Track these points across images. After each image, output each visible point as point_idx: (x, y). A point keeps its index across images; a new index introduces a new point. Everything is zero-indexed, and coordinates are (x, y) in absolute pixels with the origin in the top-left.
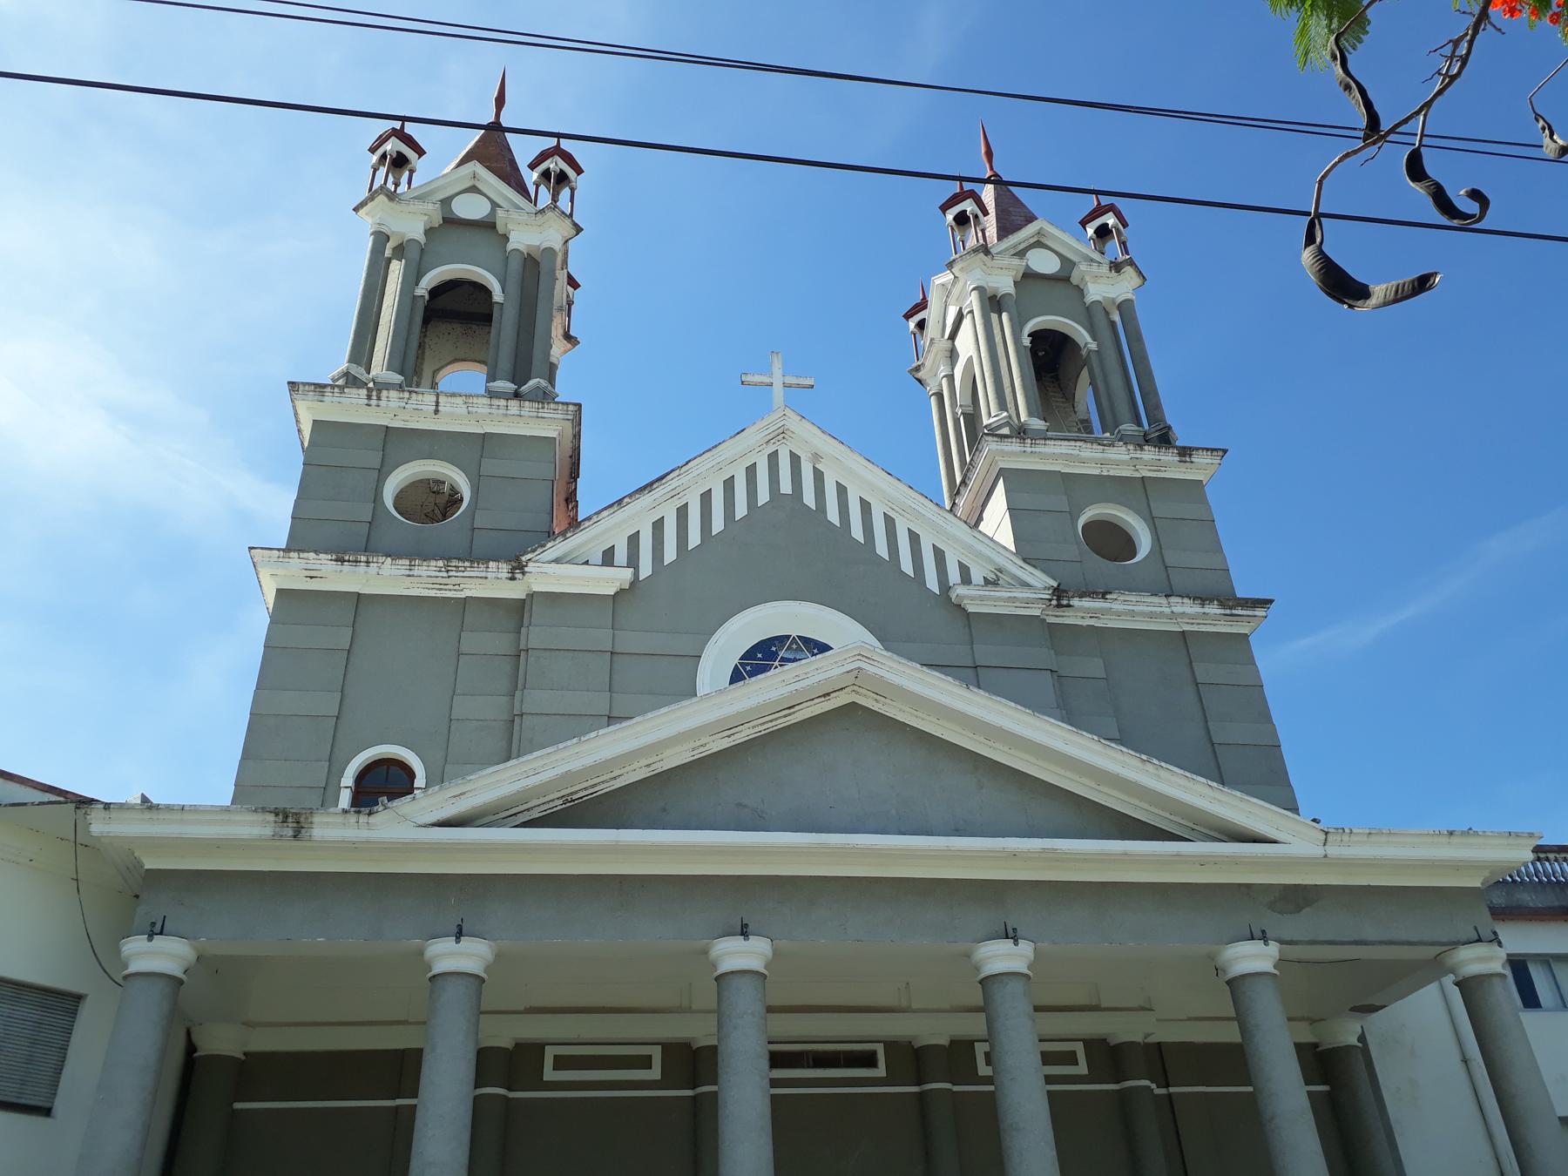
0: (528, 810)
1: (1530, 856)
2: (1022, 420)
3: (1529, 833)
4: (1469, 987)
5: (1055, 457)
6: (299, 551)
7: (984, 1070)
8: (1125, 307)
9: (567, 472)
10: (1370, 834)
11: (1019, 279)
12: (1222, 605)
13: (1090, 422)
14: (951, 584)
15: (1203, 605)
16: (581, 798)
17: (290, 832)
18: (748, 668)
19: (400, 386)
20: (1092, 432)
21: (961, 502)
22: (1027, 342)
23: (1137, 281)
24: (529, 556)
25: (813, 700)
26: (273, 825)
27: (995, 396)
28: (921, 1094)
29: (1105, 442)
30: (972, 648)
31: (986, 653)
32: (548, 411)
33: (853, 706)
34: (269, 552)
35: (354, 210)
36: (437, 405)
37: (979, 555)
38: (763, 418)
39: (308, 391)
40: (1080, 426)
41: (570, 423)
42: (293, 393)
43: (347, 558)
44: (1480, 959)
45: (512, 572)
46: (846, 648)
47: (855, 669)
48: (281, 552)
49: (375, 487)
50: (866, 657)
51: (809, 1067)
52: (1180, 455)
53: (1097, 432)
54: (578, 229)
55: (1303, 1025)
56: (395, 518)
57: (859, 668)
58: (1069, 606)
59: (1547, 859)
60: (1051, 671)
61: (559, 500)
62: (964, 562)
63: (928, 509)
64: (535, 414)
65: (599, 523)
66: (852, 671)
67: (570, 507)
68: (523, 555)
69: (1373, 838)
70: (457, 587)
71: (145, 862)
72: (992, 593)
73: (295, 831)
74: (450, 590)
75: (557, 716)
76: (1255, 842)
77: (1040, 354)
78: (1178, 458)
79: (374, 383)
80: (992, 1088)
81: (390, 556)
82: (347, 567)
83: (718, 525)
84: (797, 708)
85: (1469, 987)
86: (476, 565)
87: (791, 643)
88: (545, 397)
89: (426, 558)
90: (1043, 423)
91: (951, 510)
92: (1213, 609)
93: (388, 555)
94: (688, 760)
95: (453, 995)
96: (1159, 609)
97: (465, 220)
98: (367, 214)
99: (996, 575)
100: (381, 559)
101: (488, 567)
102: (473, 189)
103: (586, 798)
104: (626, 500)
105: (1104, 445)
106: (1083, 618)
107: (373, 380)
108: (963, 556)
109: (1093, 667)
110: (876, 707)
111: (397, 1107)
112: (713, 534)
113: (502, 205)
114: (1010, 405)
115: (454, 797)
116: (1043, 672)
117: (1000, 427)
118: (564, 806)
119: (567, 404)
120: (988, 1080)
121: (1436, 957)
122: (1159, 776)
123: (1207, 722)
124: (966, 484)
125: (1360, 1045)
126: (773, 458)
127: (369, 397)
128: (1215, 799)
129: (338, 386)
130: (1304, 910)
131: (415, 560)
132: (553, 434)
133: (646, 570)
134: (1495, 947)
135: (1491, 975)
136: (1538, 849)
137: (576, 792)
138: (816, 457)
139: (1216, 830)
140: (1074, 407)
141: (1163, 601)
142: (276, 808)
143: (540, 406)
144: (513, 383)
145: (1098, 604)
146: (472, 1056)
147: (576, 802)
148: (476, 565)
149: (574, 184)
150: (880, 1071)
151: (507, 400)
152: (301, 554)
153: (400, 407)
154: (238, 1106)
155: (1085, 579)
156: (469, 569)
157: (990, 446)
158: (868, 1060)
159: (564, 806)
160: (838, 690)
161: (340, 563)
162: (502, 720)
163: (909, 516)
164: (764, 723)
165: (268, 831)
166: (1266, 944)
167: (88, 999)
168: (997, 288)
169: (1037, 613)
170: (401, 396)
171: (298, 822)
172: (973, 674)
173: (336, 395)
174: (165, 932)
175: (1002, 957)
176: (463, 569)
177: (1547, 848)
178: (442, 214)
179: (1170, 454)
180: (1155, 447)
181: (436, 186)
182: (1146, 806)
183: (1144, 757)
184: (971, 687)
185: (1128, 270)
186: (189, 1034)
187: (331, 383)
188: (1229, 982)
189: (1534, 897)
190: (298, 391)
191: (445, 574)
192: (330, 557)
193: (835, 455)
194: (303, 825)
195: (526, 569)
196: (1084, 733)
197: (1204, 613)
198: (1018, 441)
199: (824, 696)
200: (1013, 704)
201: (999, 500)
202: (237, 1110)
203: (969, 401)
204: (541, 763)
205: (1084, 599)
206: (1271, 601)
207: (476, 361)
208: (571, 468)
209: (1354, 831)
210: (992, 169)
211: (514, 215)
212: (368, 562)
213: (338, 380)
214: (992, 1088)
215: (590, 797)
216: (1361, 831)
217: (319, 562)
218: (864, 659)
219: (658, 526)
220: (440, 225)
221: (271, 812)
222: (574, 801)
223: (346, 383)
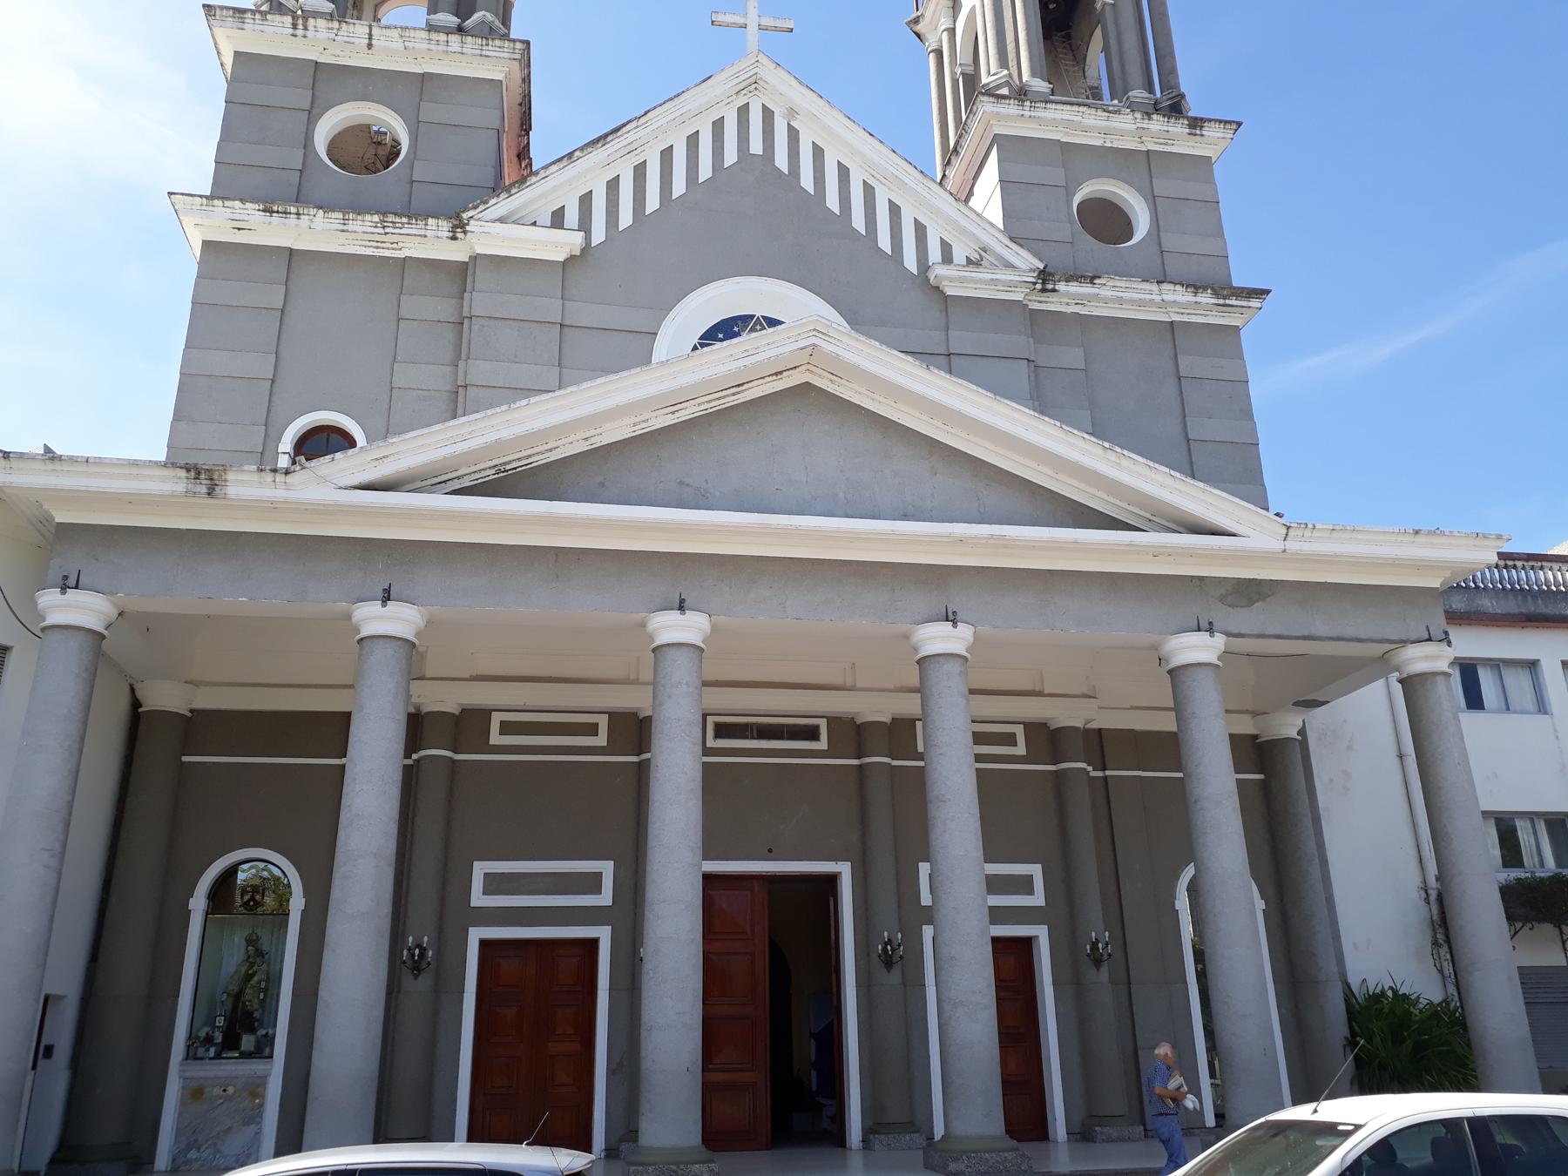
0: (458, 478)
1: (1494, 559)
2: (1024, 80)
3: (1496, 535)
4: (1413, 686)
5: (1055, 123)
6: (223, 198)
9: (517, 122)
10: (1333, 530)
12: (1216, 294)
13: (1101, 90)
14: (930, 264)
15: (1196, 293)
16: (515, 468)
17: (204, 490)
19: (331, 15)
20: (1101, 99)
21: (951, 173)
24: (470, 213)
25: (763, 378)
28: (860, 766)
29: (1111, 108)
31: (960, 340)
32: (495, 48)
33: (807, 386)
34: (191, 198)
36: (370, 39)
37: (964, 231)
39: (227, 17)
40: (1089, 92)
41: (517, 64)
42: (209, 18)
43: (275, 208)
44: (1427, 658)
45: (454, 229)
46: (800, 322)
47: (810, 346)
48: (204, 199)
49: (305, 130)
51: (753, 738)
52: (1190, 126)
53: (1106, 100)
55: (1247, 718)
57: (814, 345)
59: (1515, 567)
60: (1028, 360)
61: (508, 156)
62: (948, 240)
63: (911, 177)
64: (478, 52)
65: (546, 179)
66: (805, 347)
67: (523, 166)
68: (463, 212)
69: (1335, 534)
70: (395, 246)
71: (53, 513)
72: (973, 275)
73: (209, 489)
74: (388, 249)
75: (504, 390)
76: (1213, 534)
77: (1051, 7)
78: (1188, 131)
79: (302, 11)
80: (921, 764)
82: (276, 218)
83: (679, 187)
85: (1413, 686)
86: (414, 221)
87: (755, 324)
88: (498, 31)
89: (360, 211)
90: (1046, 84)
91: (941, 183)
92: (1206, 298)
95: (381, 657)
99: (980, 255)
100: (313, 211)
101: (426, 225)
103: (520, 469)
104: (577, 154)
105: (1109, 112)
106: (1068, 304)
107: (301, 8)
109: (1072, 357)
110: (831, 388)
112: (673, 198)
114: (1012, 63)
115: (377, 459)
116: (1020, 361)
117: (999, 87)
118: (496, 476)
121: (1383, 656)
123: (1185, 417)
125: (1299, 738)
126: (743, 111)
127: (295, 26)
128: (1176, 489)
129: (260, 12)
130: (1255, 605)
131: (349, 213)
132: (499, 76)
133: (598, 235)
134: (1444, 645)
135: (1434, 674)
136: (1501, 555)
137: (510, 462)
138: (792, 112)
140: (1084, 72)
141: (1154, 287)
142: (187, 464)
143: (484, 43)
144: (456, 16)
145: (1086, 289)
146: (403, 718)
147: (510, 472)
148: (414, 221)
151: (447, 34)
152: (226, 202)
154: (185, 759)
155: (1074, 262)
156: (406, 226)
157: (986, 106)
158: (811, 733)
159: (496, 476)
160: (791, 369)
161: (268, 214)
163: (890, 185)
164: (711, 401)
165: (180, 487)
167: (14, 650)
169: (1019, 297)
170: (330, 25)
171: (211, 479)
172: (947, 360)
173: (257, 22)
174: (80, 586)
175: (938, 638)
176: (400, 225)
177: (1516, 556)
179: (1180, 125)
180: (1164, 116)
182: (1105, 496)
183: (1107, 445)
184: (931, 368)
186: (133, 690)
187: (254, 8)
188: (1170, 672)
189: (1495, 604)
190: (214, 15)
191: (381, 231)
192: (256, 207)
193: (813, 110)
194: (217, 482)
195: (468, 228)
196: (1046, 419)
197: (1196, 302)
198: (1016, 102)
199: (776, 374)
200: (974, 387)
202: (185, 762)
203: (970, 60)
204: (468, 429)
205: (1071, 284)
206: (1267, 292)
208: (522, 118)
209: (1317, 527)
212: (298, 214)
214: (921, 764)
215: (524, 468)
216: (1324, 527)
218: (820, 335)
219: (613, 185)
221: (181, 468)
222: (507, 471)
223: (270, 9)
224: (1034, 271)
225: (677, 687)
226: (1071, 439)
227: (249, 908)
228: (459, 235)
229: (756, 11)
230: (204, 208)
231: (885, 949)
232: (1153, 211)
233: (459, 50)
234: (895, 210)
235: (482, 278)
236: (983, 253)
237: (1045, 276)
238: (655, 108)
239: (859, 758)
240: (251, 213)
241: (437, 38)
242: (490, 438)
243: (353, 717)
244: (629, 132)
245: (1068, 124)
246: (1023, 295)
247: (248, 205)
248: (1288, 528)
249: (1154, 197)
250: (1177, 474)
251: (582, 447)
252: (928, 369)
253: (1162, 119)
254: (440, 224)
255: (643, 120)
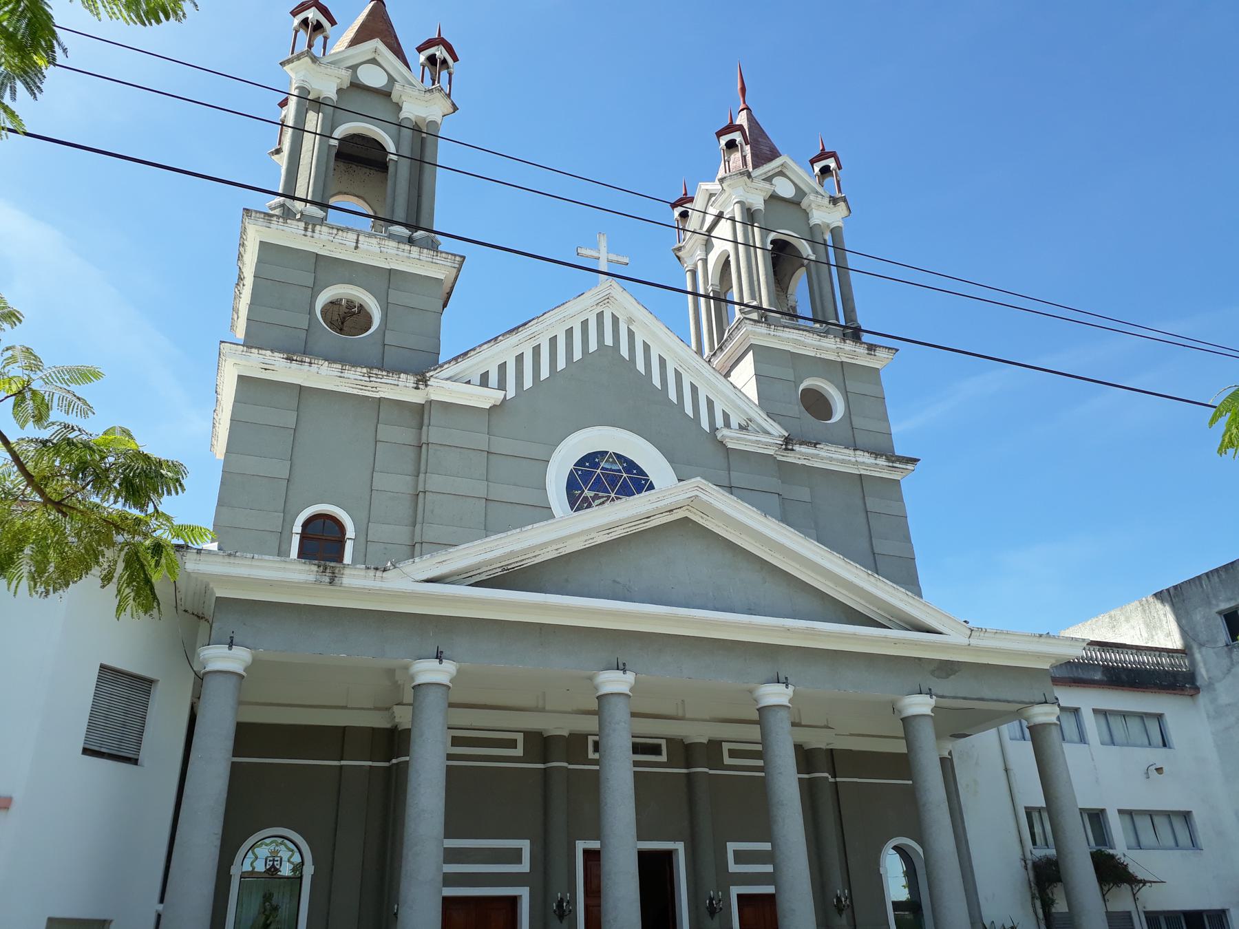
0: (479, 574)
7: (592, 755)
8: (835, 232)
11: (767, 198)
12: (888, 460)
15: (876, 458)
16: (513, 568)
17: (327, 580)
18: (580, 473)
22: (770, 247)
23: (845, 213)
24: (431, 373)
26: (315, 573)
27: (748, 288)
28: (688, 775)
30: (729, 474)
31: (737, 478)
32: (439, 259)
34: (236, 346)
35: (281, 64)
36: (357, 243)
37: (739, 407)
38: (597, 286)
42: (245, 217)
43: (295, 358)
44: (1046, 714)
50: (702, 489)
52: (868, 349)
54: (455, 108)
56: (323, 326)
57: (697, 496)
58: (792, 450)
64: (431, 260)
68: (428, 372)
69: (997, 636)
70: (374, 389)
72: (746, 436)
73: (330, 579)
76: (928, 632)
78: (866, 352)
80: (597, 768)
81: (327, 361)
82: (294, 364)
83: (561, 364)
84: (652, 518)
86: (391, 375)
89: (355, 364)
92: (882, 462)
93: (326, 360)
94: (582, 548)
96: (847, 458)
97: (367, 86)
98: (291, 69)
99: (747, 423)
101: (399, 378)
102: (373, 61)
104: (500, 338)
105: (821, 336)
106: (799, 459)
108: (726, 407)
109: (803, 493)
111: (341, 766)
113: (398, 80)
118: (502, 573)
119: (455, 255)
120: (596, 762)
122: (876, 585)
124: (722, 350)
126: (600, 316)
127: (306, 229)
133: (511, 393)
135: (1050, 724)
137: (511, 564)
138: (630, 320)
139: (906, 623)
141: (851, 452)
143: (435, 254)
145: (811, 450)
148: (391, 375)
149: (452, 70)
150: (663, 758)
151: (399, 242)
152: (260, 351)
153: (329, 240)
155: (801, 430)
159: (502, 573)
162: (409, 494)
163: (693, 374)
165: (312, 578)
166: (931, 697)
168: (752, 203)
173: (280, 223)
175: (775, 695)
176: (381, 376)
178: (351, 78)
180: (853, 341)
181: (345, 56)
183: (870, 572)
184: (768, 516)
185: (842, 204)
191: (367, 379)
192: (282, 356)
194: (337, 575)
195: (429, 383)
198: (766, 326)
201: (748, 362)
205: (802, 446)
206: (919, 460)
207: (356, 196)
210: (744, 102)
211: (408, 90)
212: (310, 363)
213: (275, 208)
214: (597, 768)
217: (273, 358)
219: (520, 359)
220: (348, 88)
222: (509, 570)
224: (782, 437)
225: (618, 724)
226: (849, 567)
227: (270, 873)
228: (421, 386)
229: (605, 249)
230: (244, 353)
231: (711, 903)
232: (845, 398)
233: (418, 257)
234: (694, 389)
235: (436, 416)
236: (749, 422)
237: (788, 441)
238: (549, 311)
239: (687, 768)
240: (277, 359)
241: (403, 248)
242: (508, 550)
243: (1027, 805)
244: (532, 326)
245: (796, 341)
246: (774, 452)
247: (276, 354)
248: (972, 630)
249: (847, 392)
250: (910, 594)
251: (554, 555)
252: (766, 517)
253: (852, 343)
254: (409, 378)
255: (540, 319)
